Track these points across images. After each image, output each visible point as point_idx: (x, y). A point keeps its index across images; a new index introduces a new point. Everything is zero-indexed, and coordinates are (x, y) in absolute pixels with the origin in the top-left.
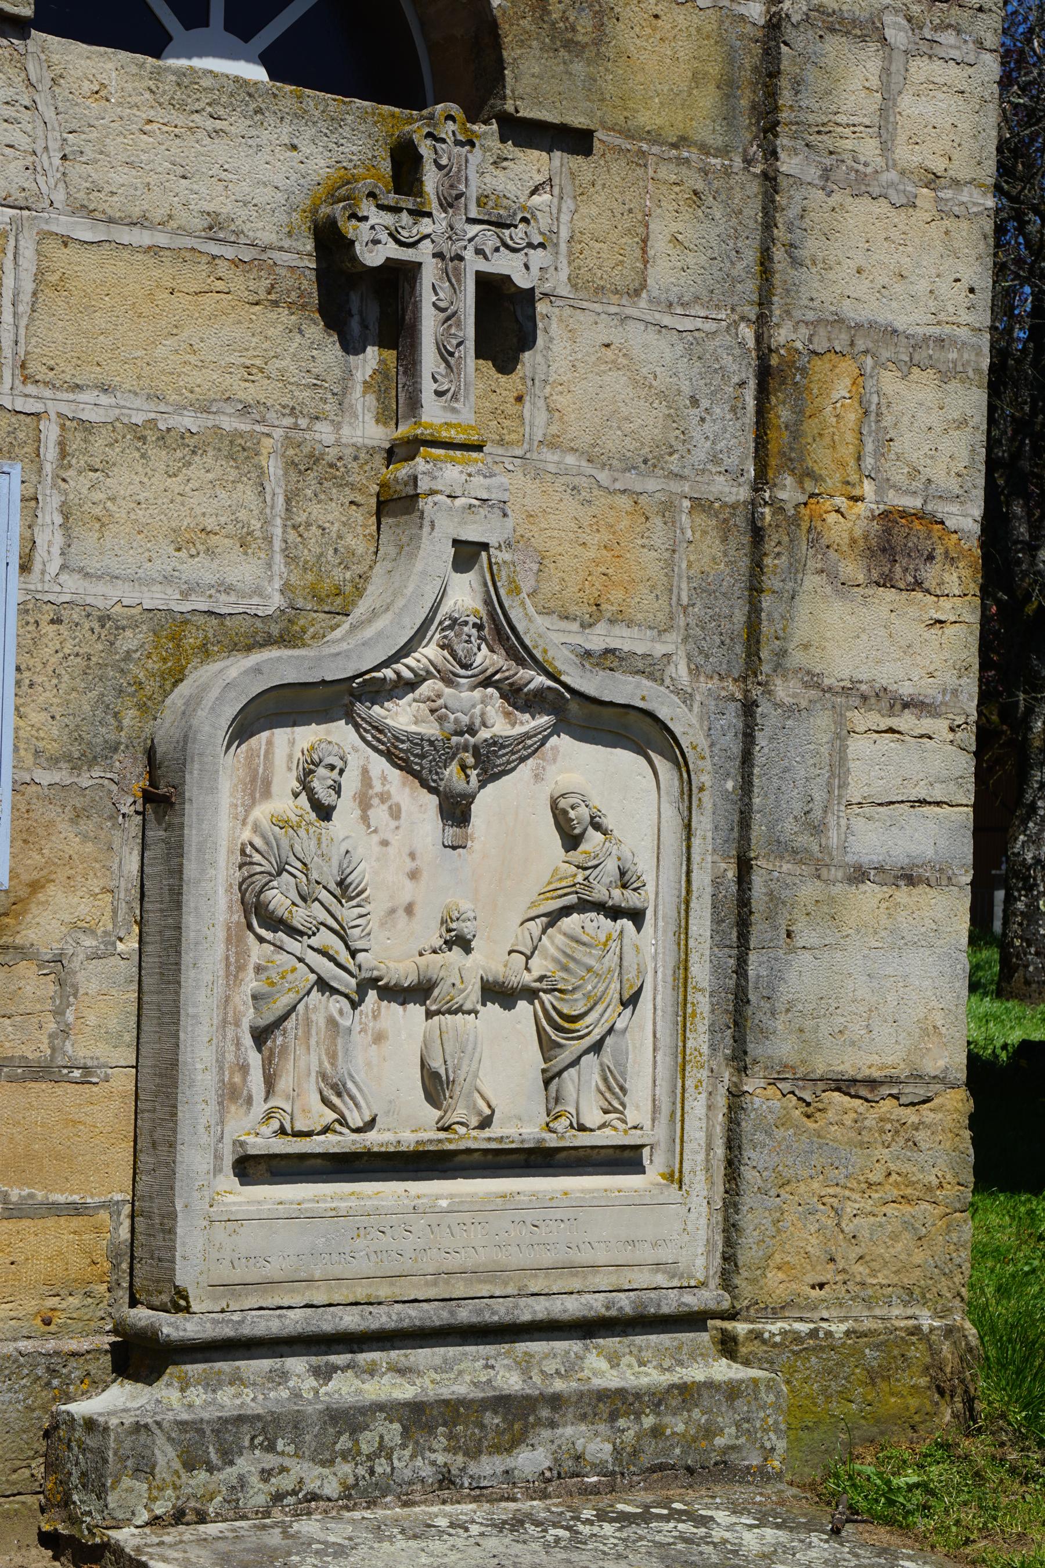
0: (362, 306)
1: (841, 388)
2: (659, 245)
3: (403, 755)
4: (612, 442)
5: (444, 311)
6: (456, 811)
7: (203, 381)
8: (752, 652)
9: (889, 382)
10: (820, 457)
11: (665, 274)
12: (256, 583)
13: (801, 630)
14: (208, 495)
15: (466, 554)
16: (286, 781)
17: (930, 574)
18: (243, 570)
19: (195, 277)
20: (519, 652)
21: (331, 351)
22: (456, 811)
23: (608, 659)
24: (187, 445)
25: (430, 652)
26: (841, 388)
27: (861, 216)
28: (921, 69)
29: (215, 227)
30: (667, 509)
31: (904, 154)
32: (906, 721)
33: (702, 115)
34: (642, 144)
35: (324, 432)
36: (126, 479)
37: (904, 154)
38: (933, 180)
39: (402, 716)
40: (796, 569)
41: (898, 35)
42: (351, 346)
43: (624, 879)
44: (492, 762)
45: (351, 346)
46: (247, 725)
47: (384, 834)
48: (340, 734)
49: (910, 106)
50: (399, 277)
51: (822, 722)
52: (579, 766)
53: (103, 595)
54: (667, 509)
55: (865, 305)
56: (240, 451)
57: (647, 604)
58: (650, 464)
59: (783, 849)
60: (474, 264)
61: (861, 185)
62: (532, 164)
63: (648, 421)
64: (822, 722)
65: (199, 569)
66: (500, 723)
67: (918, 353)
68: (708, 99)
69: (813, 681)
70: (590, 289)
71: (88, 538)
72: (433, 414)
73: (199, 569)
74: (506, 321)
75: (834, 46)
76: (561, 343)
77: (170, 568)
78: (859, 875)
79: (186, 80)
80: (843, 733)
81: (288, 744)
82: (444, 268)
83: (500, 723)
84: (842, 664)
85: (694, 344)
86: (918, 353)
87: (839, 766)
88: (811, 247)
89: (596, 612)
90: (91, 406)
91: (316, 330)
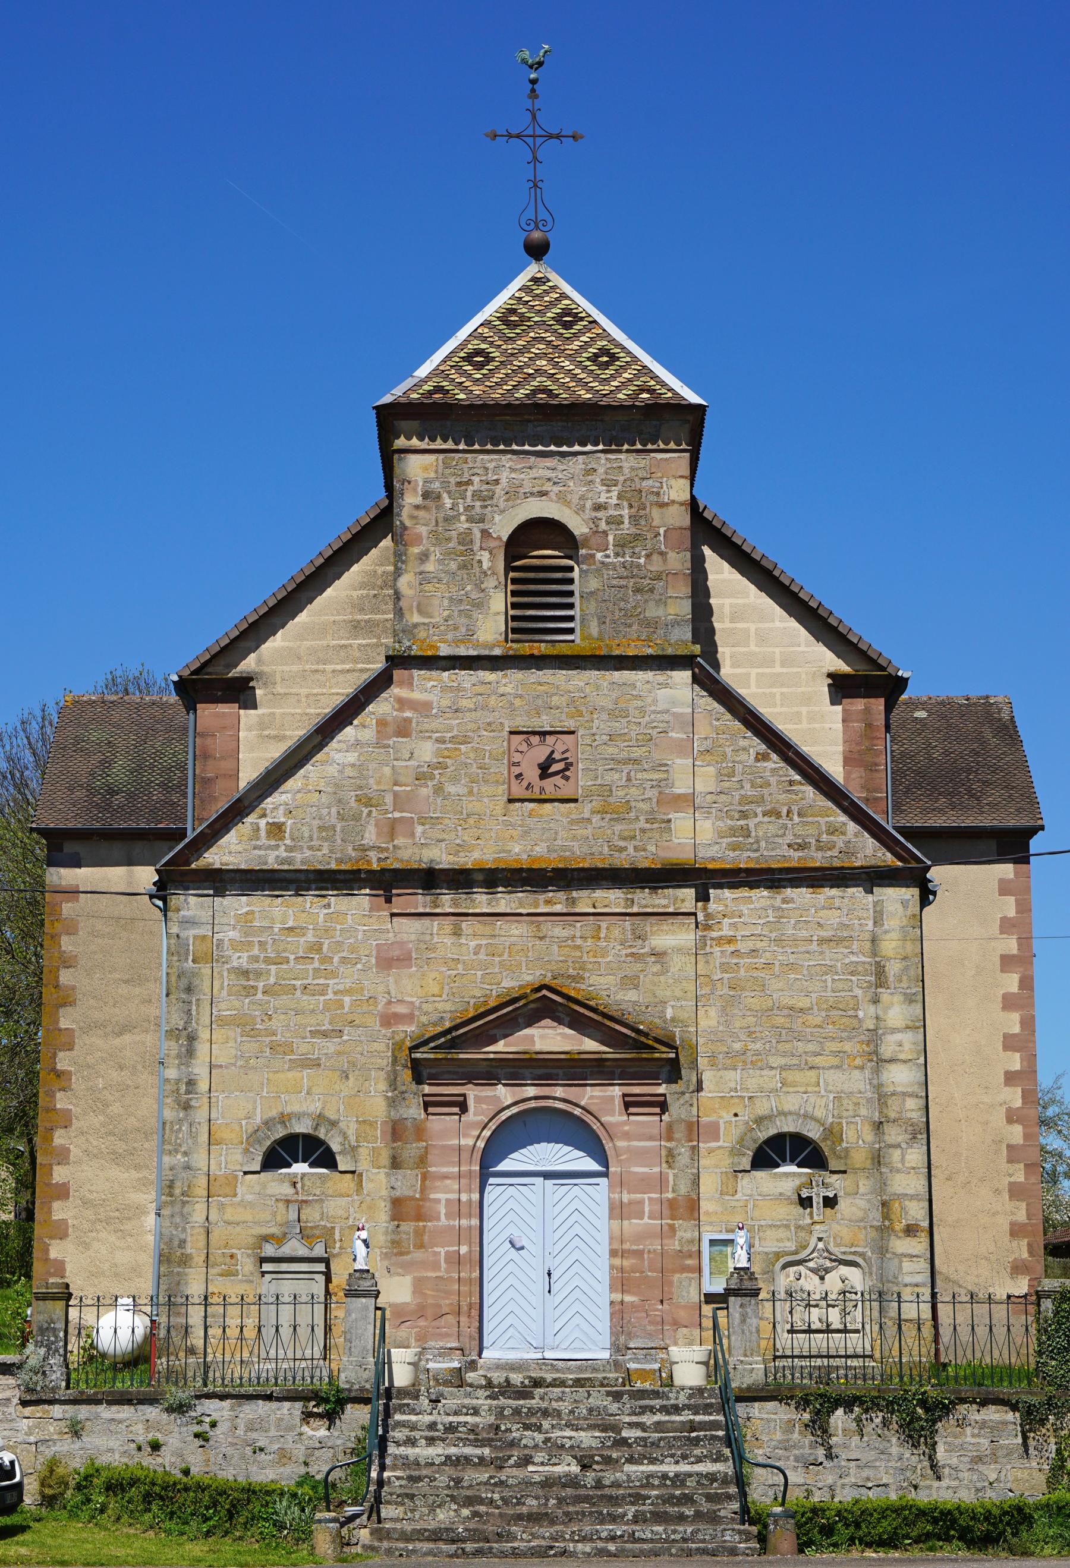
0: (806, 1203)
1: (897, 1205)
2: (861, 1185)
3: (811, 1270)
4: (854, 1218)
5: (817, 1201)
6: (822, 1278)
7: (781, 1217)
8: (882, 1251)
9: (907, 1203)
10: (893, 1217)
11: (862, 1190)
12: (791, 1246)
13: (891, 1245)
14: (782, 1233)
15: (820, 1239)
16: (792, 1275)
17: (918, 1234)
18: (788, 1244)
19: (778, 1202)
20: (830, 1253)
21: (802, 1209)
22: (822, 1278)
23: (844, 1253)
24: (779, 1227)
25: (815, 1254)
26: (897, 1205)
27: (898, 1176)
28: (909, 1151)
29: (781, 1194)
30: (865, 1228)
31: (907, 1165)
32: (914, 1259)
33: (868, 1164)
34: (856, 1170)
35: (801, 1222)
36: (768, 1232)
37: (907, 1165)
38: (914, 1168)
39: (811, 1264)
40: (889, 1235)
41: (904, 1145)
42: (805, 1209)
43: (852, 1287)
44: (827, 1271)
45: (805, 1209)
46: (785, 1266)
47: (810, 1283)
48: (801, 1268)
49: (908, 1157)
50: (810, 1199)
51: (896, 1261)
52: (844, 1270)
53: (766, 1250)
54: (865, 1228)
55: (900, 1190)
56: (787, 1227)
57: (862, 1243)
58: (862, 1221)
59: (889, 1281)
60: (822, 1194)
61: (898, 1171)
62: (836, 1176)
63: (860, 1214)
64: (896, 1261)
65: (781, 1245)
66: (828, 1264)
67: (912, 1197)
68: (869, 1161)
69: (894, 1253)
70: (847, 1194)
71: (763, 1242)
72: (816, 1218)
73: (781, 1245)
74: (830, 1202)
75: (891, 1150)
76: (842, 1204)
77: (241, 1415)
78: (906, 1285)
79: (775, 1174)
80: (901, 1262)
81: (792, 1270)
82: (817, 1195)
83: (828, 1264)
84: (900, 1251)
85: (869, 1201)
86: (912, 1197)
87: (901, 1268)
88: (889, 1182)
89: (852, 1245)
90: (763, 1223)
91: (799, 1207)
